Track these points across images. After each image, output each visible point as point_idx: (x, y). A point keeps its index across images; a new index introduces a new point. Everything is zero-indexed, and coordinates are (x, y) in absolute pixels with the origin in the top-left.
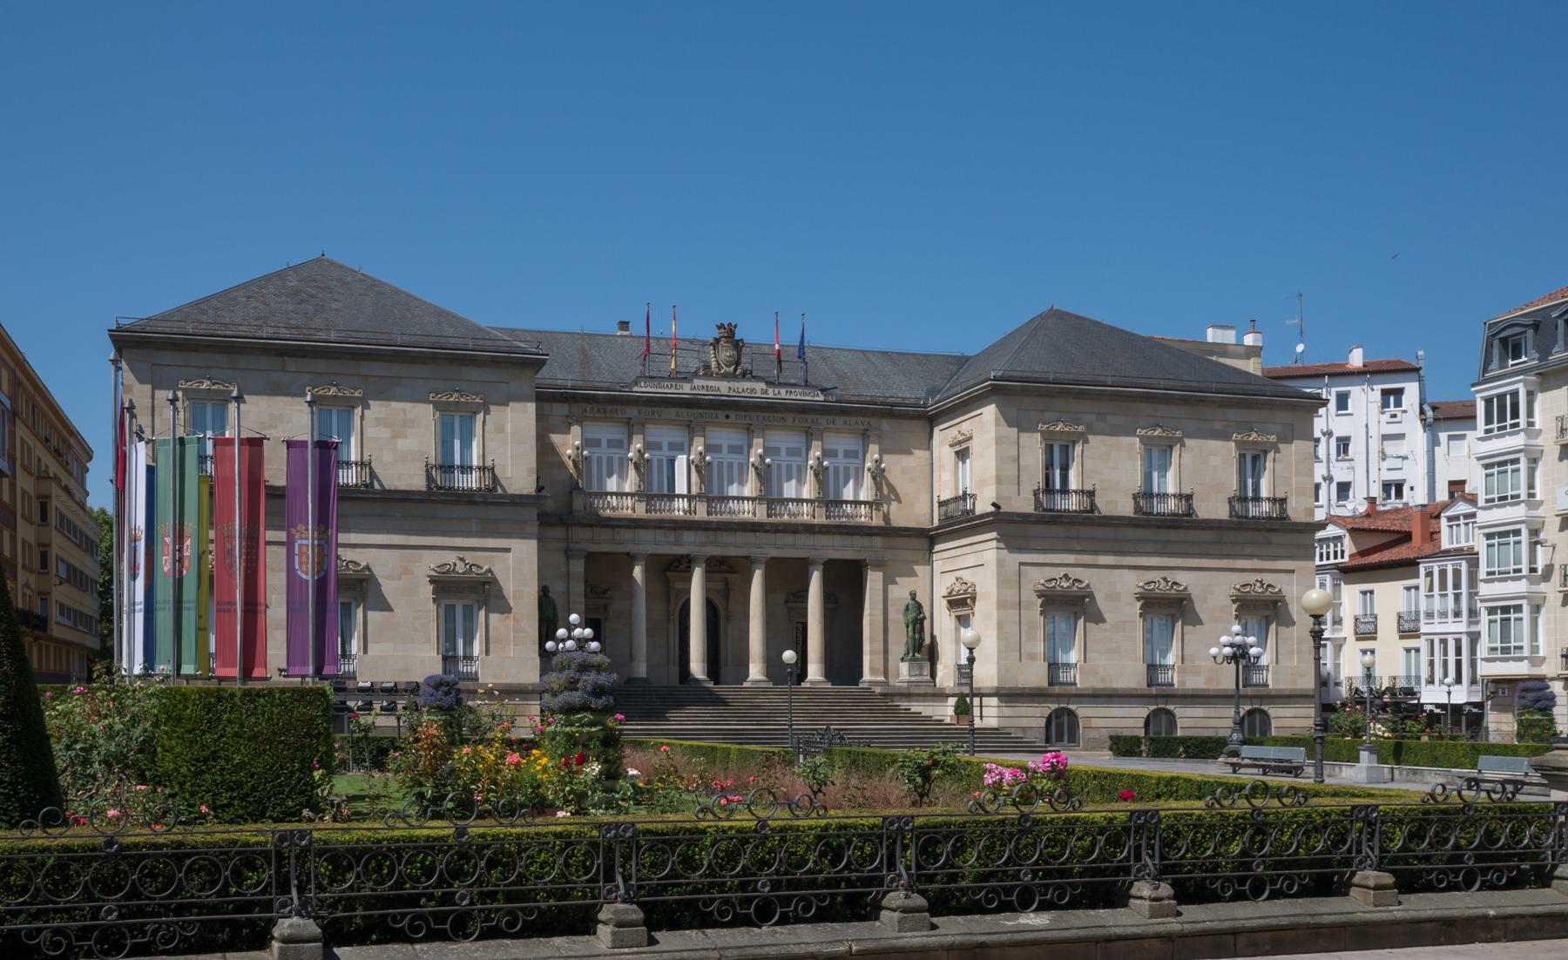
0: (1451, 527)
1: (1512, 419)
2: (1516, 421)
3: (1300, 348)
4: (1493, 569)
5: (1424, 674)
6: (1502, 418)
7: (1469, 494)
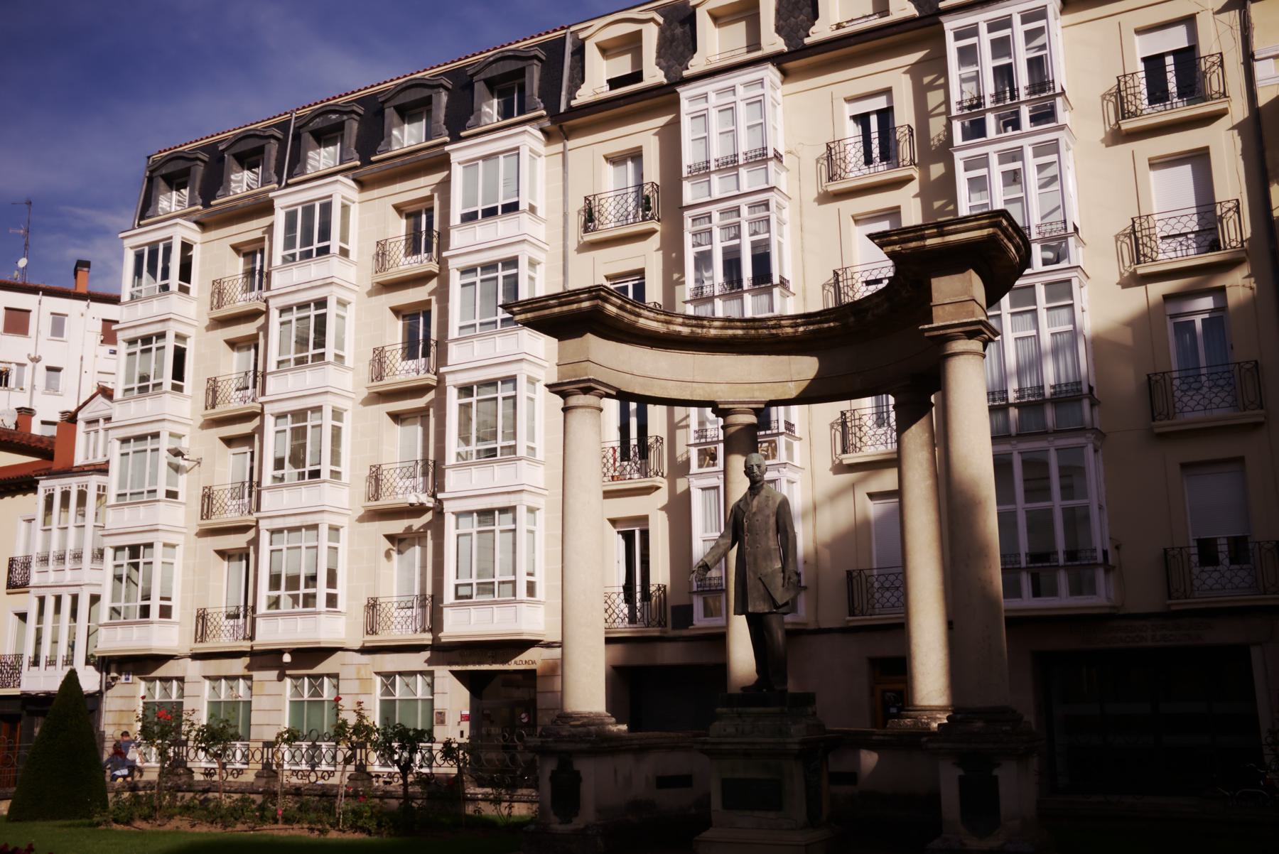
0: (88, 433)
1: (319, 241)
2: (326, 244)
3: (23, 263)
4: (123, 492)
5: (29, 652)
6: (307, 240)
7: (416, 417)
